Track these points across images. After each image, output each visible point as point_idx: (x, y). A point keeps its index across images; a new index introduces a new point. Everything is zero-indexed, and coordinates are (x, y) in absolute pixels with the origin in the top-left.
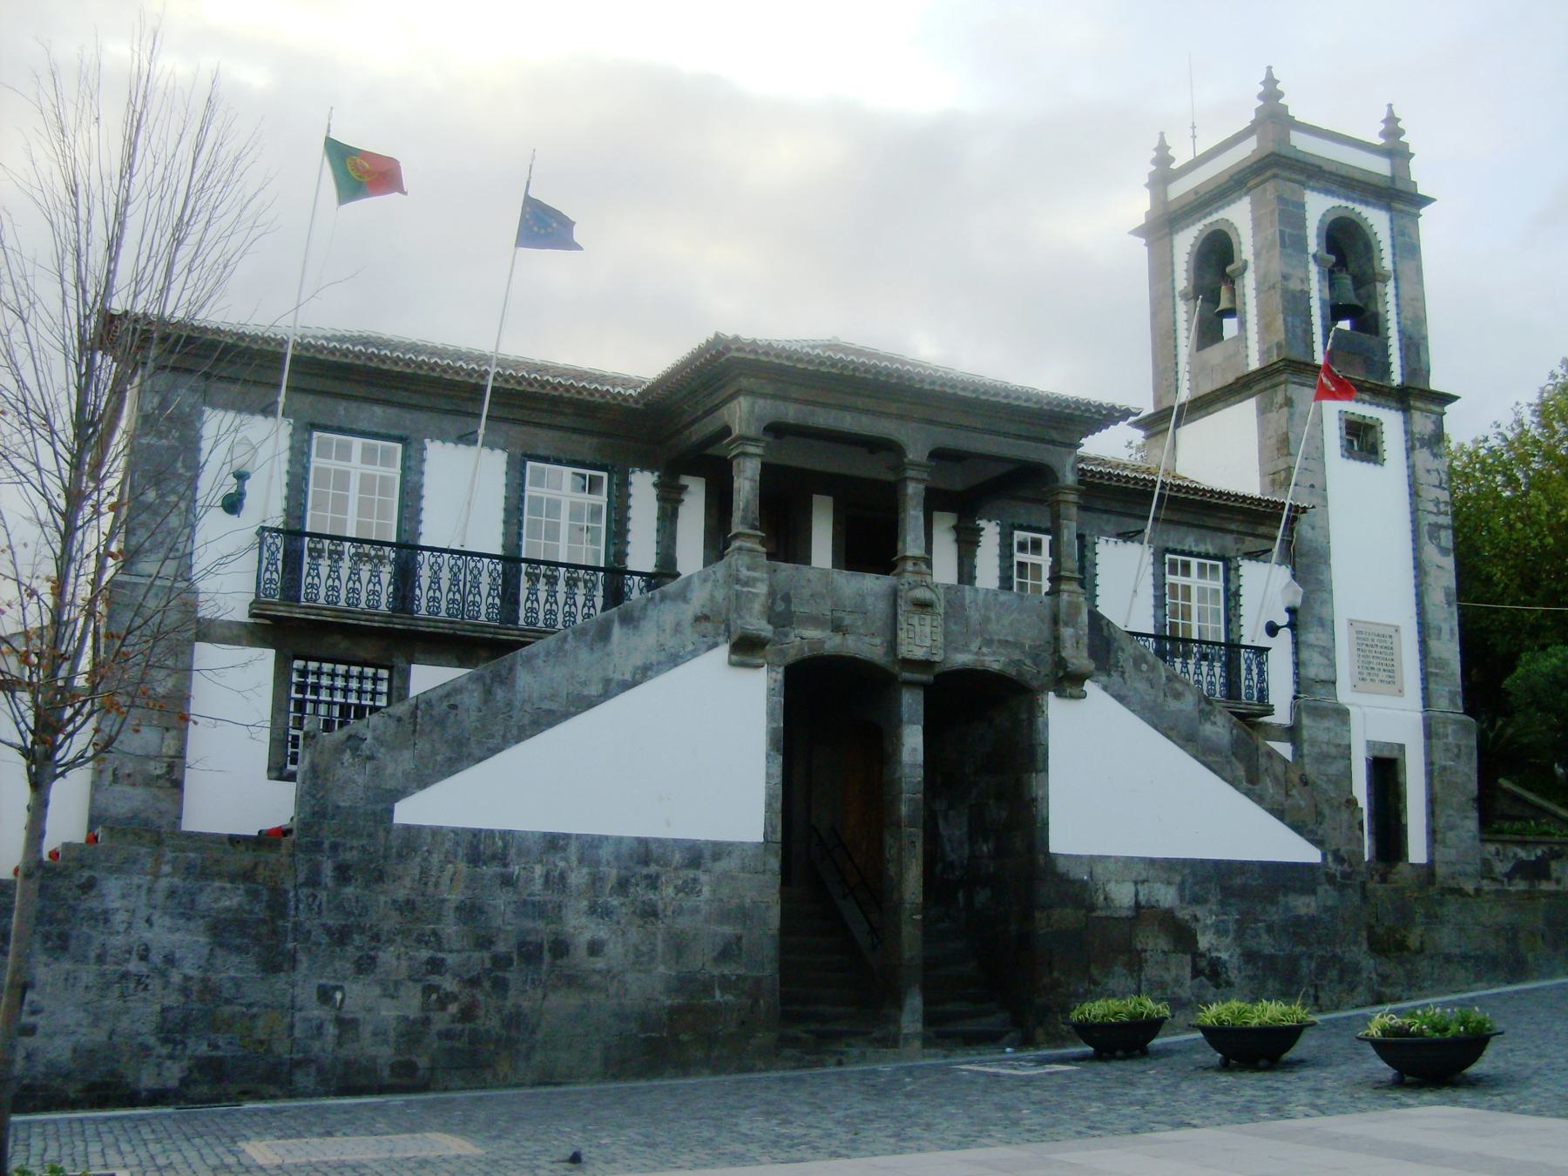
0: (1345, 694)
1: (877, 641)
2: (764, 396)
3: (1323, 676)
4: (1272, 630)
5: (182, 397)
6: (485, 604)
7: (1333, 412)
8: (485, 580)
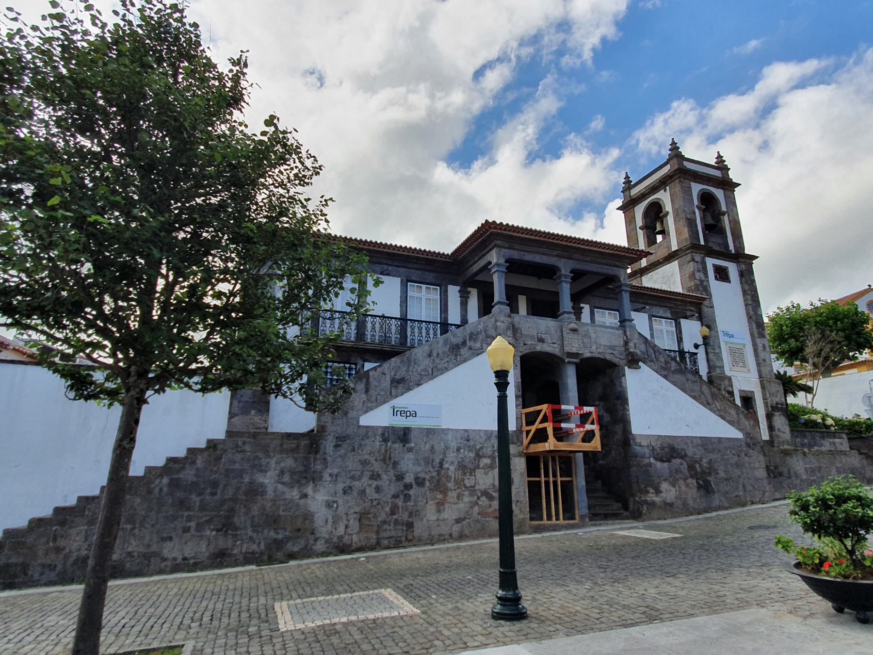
0: (728, 373)
1: (556, 345)
2: (504, 247)
4: (696, 346)
6: (394, 337)
7: (710, 262)
8: (393, 328)
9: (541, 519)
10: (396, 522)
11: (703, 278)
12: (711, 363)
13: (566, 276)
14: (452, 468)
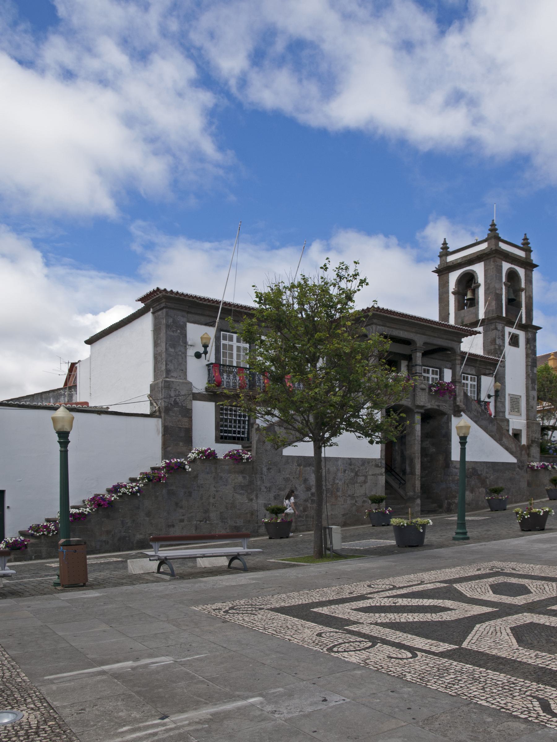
0: (507, 416)
1: (409, 400)
2: (380, 325)
3: (502, 410)
4: (489, 396)
5: (181, 319)
10: (307, 516)
11: (501, 344)
12: (497, 409)
14: (340, 483)
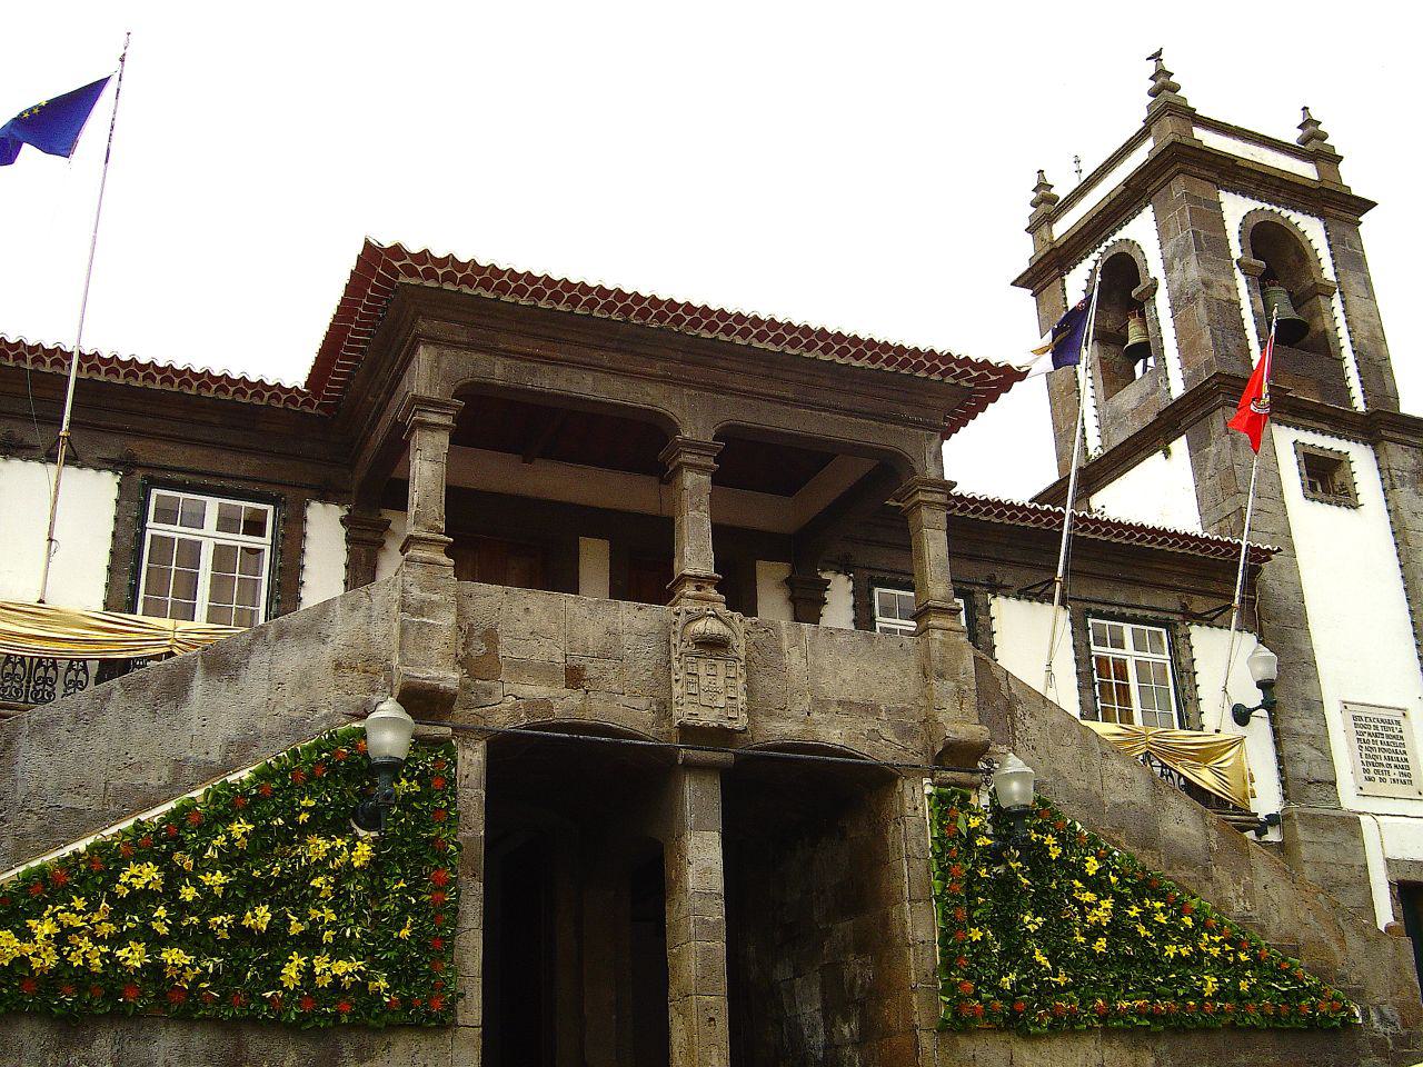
0: (1349, 799)
1: (643, 702)
2: (453, 345)
3: (1317, 774)
4: (1242, 716)
7: (1285, 441)
9: (134, 612)
13: (697, 447)
